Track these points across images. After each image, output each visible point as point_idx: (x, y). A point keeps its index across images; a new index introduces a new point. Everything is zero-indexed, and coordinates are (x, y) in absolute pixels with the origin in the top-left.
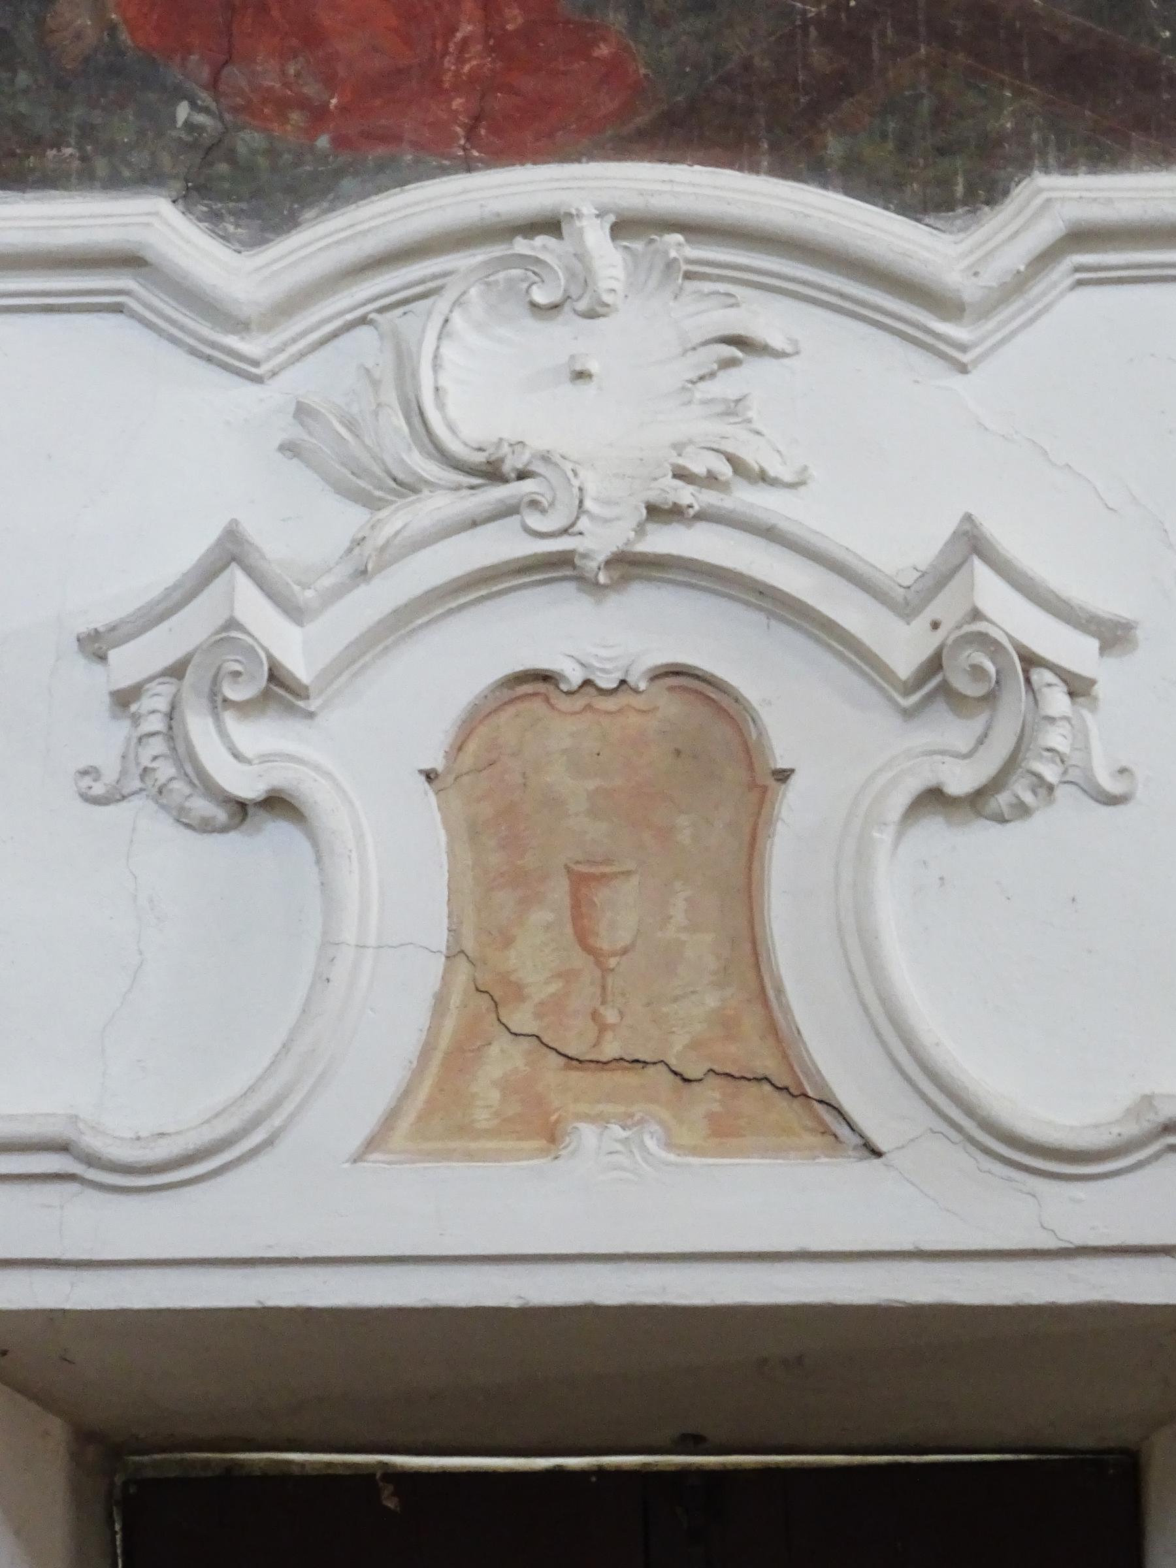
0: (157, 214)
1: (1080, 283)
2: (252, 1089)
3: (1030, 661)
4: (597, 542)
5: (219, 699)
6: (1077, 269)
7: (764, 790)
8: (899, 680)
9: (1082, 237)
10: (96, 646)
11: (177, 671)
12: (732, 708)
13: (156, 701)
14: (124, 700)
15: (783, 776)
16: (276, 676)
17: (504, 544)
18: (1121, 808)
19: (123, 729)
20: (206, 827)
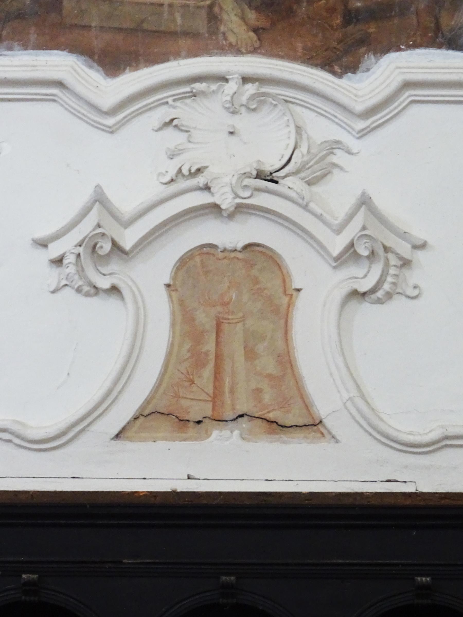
3: (386, 249)
10: (43, 244)
13: (70, 259)
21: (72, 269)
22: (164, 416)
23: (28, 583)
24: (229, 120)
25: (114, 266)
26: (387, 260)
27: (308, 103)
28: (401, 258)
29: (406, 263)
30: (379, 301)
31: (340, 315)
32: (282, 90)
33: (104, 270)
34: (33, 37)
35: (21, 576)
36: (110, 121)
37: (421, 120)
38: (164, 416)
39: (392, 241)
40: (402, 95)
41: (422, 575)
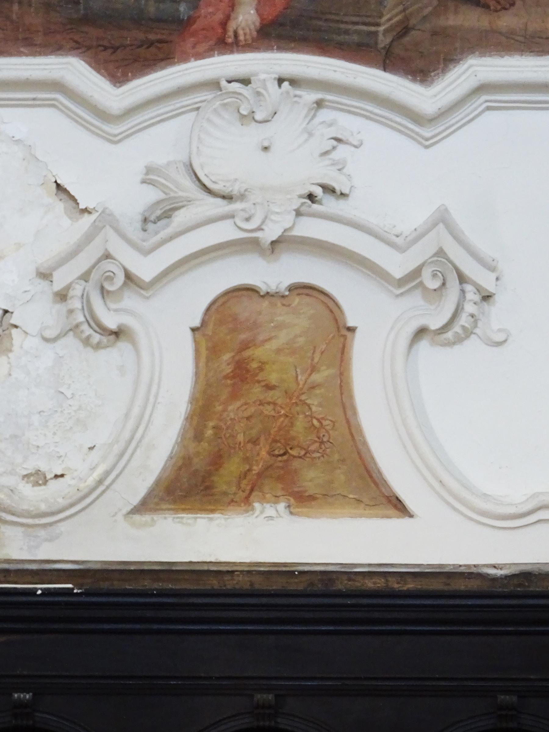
0: (475, 71)
1: (489, 108)
2: (127, 416)
3: (462, 279)
4: (271, 233)
5: (105, 292)
6: (487, 101)
7: (345, 337)
8: (394, 278)
9: (483, 88)
10: (45, 275)
11: (85, 277)
12: (335, 309)
13: (77, 290)
14: (62, 296)
15: (352, 330)
16: (129, 277)
17: (225, 232)
18: (506, 344)
19: (62, 308)
20: (98, 347)
21: (77, 304)
22: (190, 486)
23: (21, 705)
24: (263, 135)
25: (130, 300)
26: (463, 291)
27: (145, 121)
28: (479, 289)
29: (487, 297)
30: (450, 344)
31: (407, 359)
32: (158, 110)
33: (113, 306)
34: (235, 50)
35: (11, 695)
36: (427, 132)
37: (494, 127)
38: (190, 486)
39: (470, 268)
40: (89, 115)
41: (174, 684)
